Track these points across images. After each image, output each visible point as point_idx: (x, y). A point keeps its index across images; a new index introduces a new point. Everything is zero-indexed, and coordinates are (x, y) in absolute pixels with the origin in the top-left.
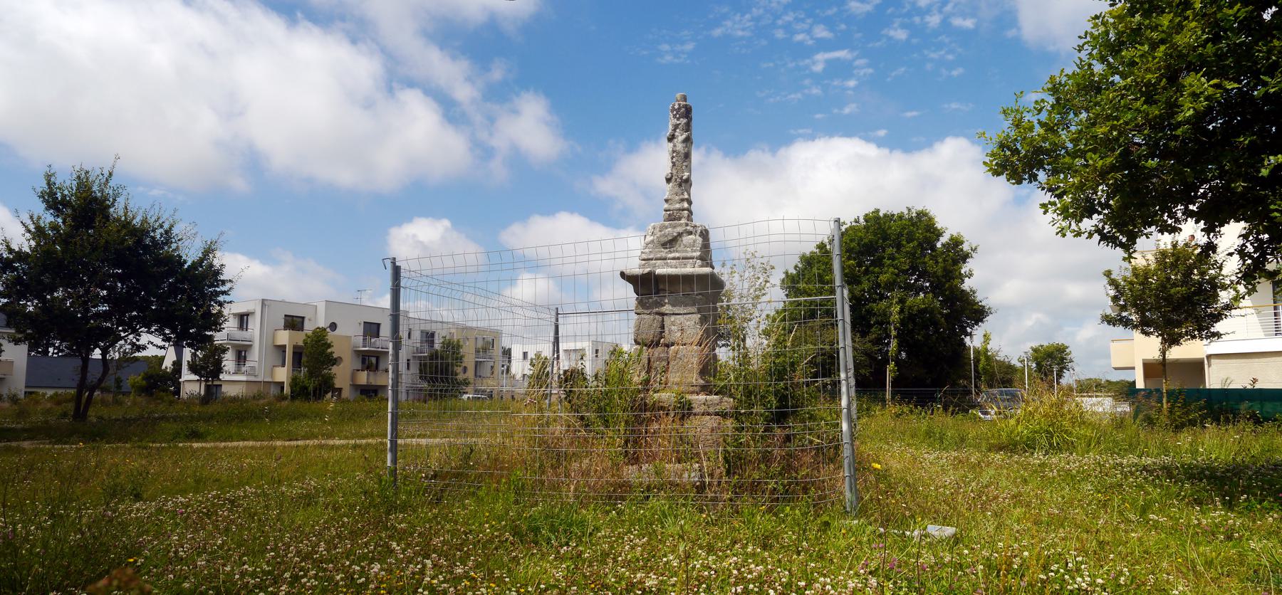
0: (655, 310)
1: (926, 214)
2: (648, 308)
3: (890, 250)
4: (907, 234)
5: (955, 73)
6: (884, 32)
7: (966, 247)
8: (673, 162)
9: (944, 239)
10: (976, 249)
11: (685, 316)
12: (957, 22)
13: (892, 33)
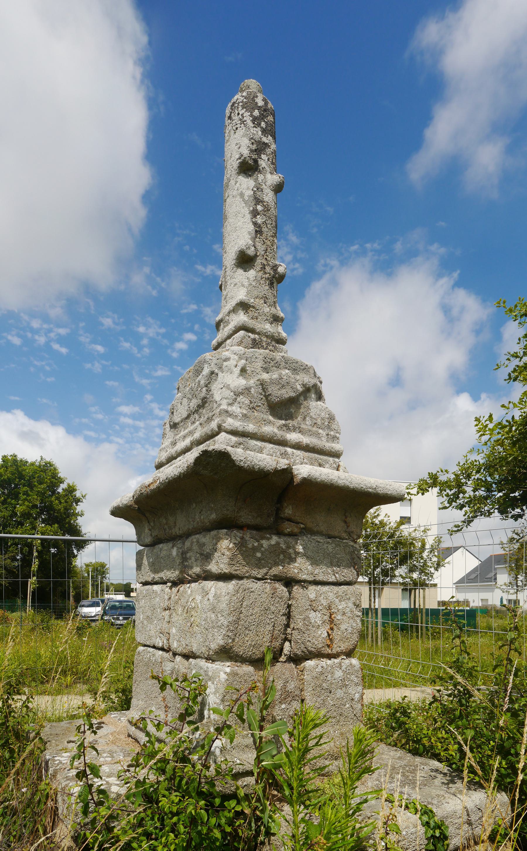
0: (277, 570)
1: (51, 465)
2: (259, 564)
3: (25, 489)
4: (38, 477)
5: (49, 380)
6: (5, 334)
7: (78, 494)
8: (255, 224)
9: (63, 486)
10: (85, 496)
11: (336, 588)
12: (56, 346)
13: (10, 337)
